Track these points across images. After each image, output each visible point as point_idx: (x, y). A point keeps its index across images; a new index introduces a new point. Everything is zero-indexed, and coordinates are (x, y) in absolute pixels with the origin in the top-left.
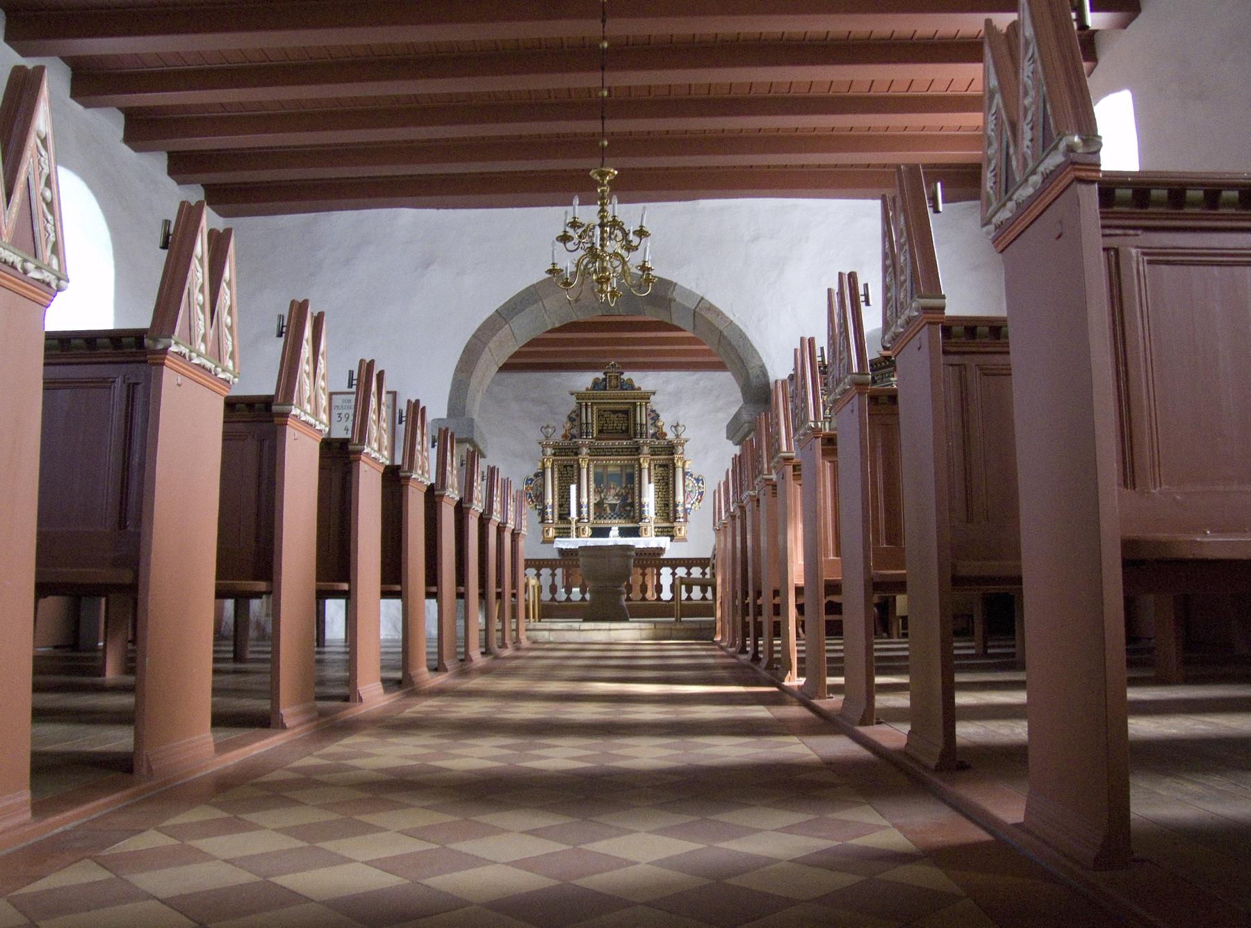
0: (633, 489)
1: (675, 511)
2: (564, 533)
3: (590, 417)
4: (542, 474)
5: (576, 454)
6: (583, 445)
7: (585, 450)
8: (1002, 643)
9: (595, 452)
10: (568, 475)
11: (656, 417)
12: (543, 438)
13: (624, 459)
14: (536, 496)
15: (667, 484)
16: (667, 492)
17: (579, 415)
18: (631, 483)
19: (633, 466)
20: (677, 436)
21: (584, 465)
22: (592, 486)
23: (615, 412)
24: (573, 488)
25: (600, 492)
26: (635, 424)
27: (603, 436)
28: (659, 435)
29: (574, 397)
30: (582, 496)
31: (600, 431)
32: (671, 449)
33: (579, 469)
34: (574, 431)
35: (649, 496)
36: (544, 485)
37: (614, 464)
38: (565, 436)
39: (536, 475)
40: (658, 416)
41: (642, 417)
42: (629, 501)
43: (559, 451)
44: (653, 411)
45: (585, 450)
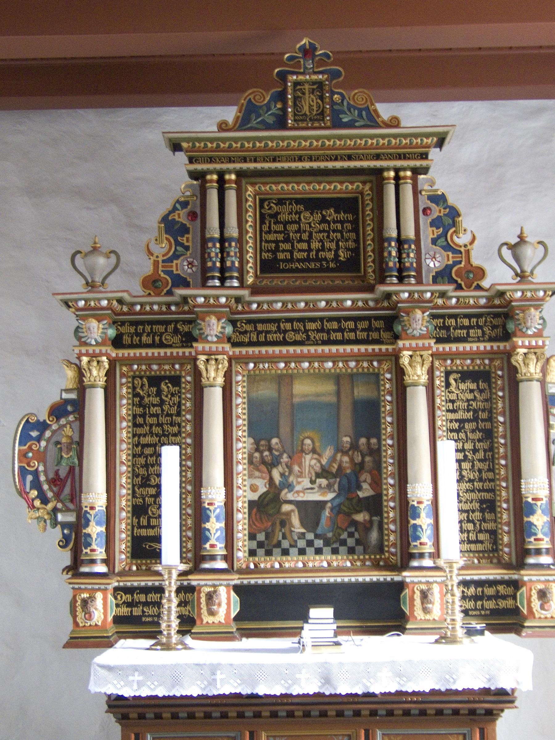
0: (376, 453)
1: (522, 530)
2: (138, 619)
3: (234, 217)
4: (72, 408)
5: (189, 339)
6: (211, 308)
7: (215, 327)
8: (25, 63)
9: (249, 332)
10: (162, 409)
11: (449, 219)
12: (76, 284)
13: (348, 356)
14: (56, 481)
15: (489, 435)
16: (490, 458)
17: (199, 215)
18: (371, 428)
19: (375, 378)
20: (522, 276)
21: (214, 375)
22: (243, 445)
23: (314, 204)
24: (170, 457)
25: (271, 465)
26: (381, 240)
27: (277, 280)
28: (462, 273)
29: (182, 157)
30: (217, 473)
31: (267, 266)
32: (501, 319)
33: (199, 391)
34: (182, 267)
35: (437, 477)
36: (79, 445)
37: (312, 375)
38: (152, 283)
39: (58, 411)
40: (454, 213)
41: (402, 216)
42: (366, 491)
43: (131, 328)
44: (439, 199)
45: (420, 322)
